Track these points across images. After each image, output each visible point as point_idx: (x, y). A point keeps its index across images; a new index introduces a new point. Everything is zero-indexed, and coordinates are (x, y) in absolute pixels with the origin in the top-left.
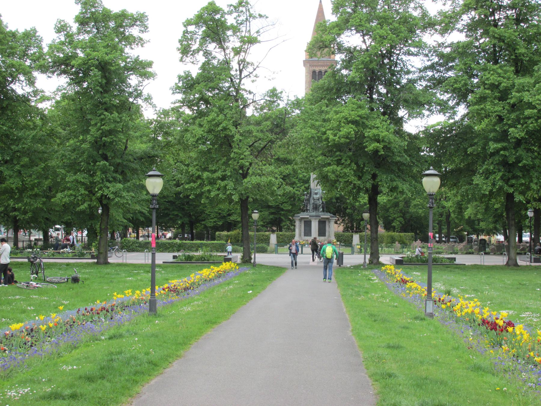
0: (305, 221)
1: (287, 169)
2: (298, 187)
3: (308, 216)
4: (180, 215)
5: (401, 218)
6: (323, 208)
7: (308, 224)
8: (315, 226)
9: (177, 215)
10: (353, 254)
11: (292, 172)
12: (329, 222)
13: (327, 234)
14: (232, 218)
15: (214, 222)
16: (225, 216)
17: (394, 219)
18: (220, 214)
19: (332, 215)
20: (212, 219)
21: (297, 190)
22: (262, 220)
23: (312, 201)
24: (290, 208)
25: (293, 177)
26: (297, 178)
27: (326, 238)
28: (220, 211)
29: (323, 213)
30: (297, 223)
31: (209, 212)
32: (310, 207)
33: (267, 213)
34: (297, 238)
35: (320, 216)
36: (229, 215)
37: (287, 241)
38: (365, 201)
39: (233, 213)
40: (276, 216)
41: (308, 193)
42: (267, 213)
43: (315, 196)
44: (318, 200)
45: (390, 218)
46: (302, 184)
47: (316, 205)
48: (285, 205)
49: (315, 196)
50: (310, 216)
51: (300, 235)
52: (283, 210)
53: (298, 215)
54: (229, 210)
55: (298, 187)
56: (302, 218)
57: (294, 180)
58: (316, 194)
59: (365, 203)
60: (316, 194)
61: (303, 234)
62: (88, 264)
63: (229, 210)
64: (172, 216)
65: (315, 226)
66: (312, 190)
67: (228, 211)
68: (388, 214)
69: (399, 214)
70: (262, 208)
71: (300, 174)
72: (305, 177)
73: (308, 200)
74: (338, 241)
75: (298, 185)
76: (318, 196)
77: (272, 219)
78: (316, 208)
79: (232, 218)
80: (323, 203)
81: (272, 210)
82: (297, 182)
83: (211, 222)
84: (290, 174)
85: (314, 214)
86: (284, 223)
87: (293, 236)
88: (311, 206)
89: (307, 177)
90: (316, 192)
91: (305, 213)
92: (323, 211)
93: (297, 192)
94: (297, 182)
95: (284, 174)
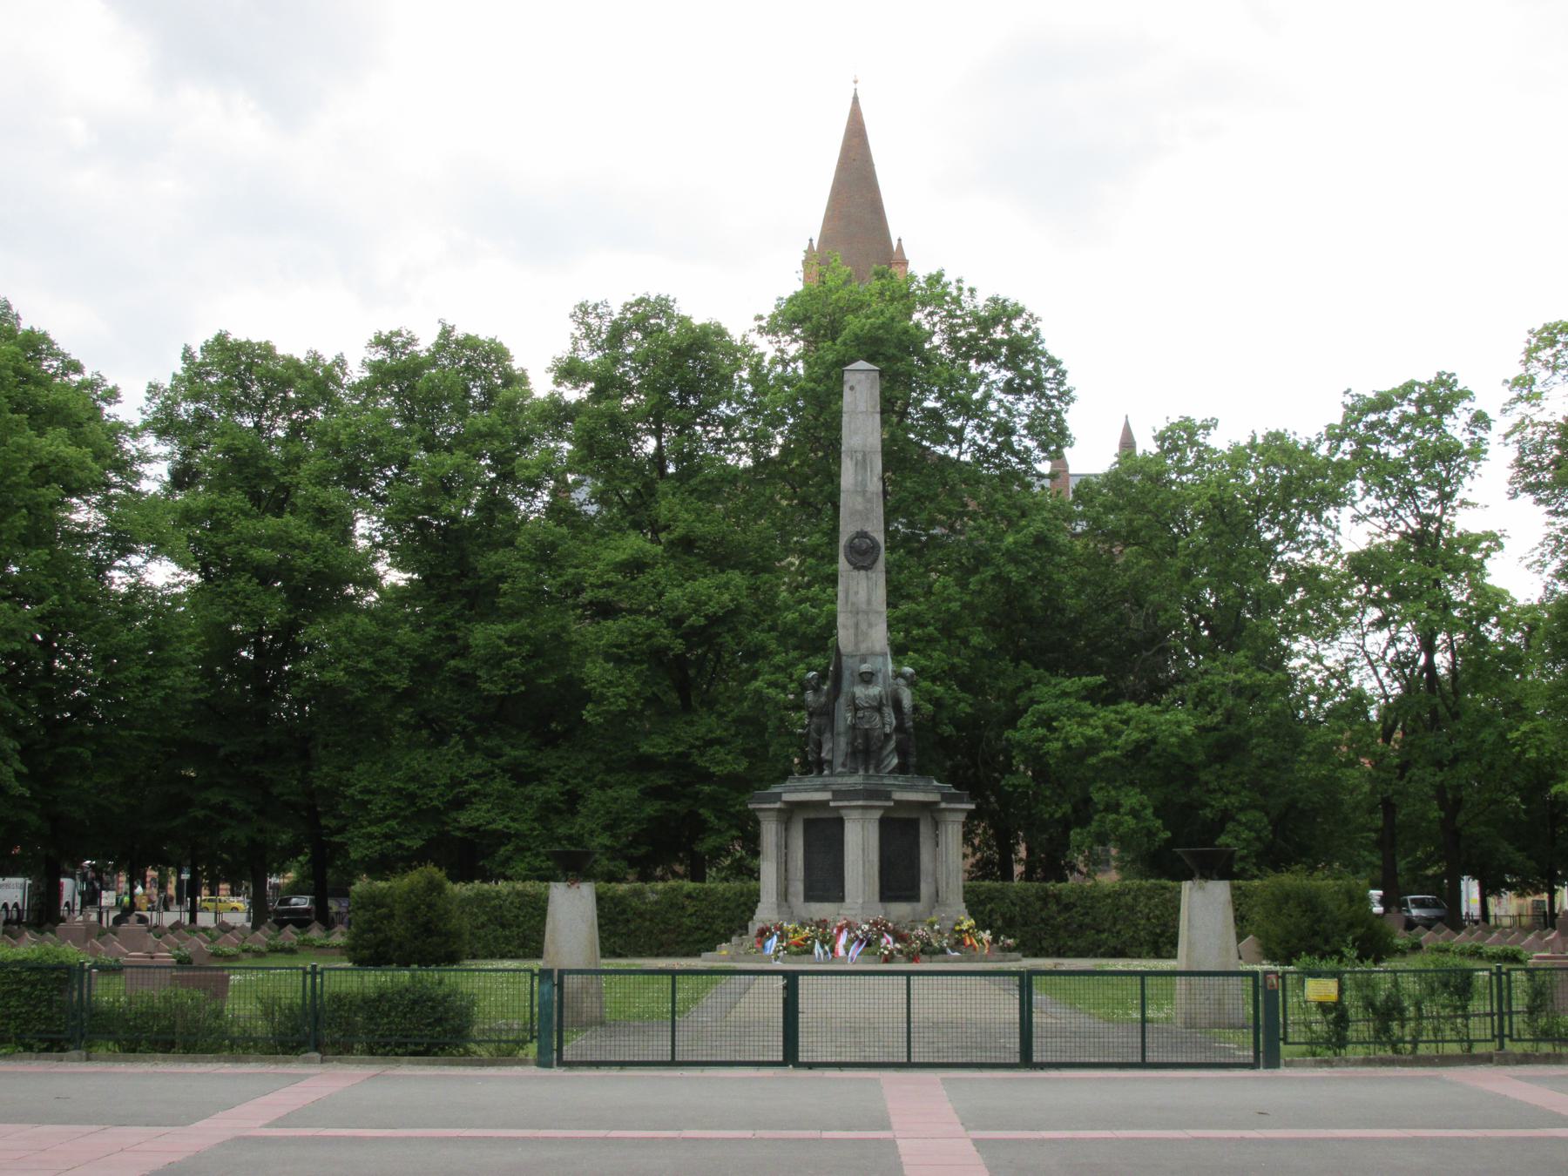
0: (809, 825)
1: (726, 586)
2: (778, 668)
3: (826, 796)
4: (237, 805)
5: (1258, 814)
6: (901, 751)
7: (824, 836)
8: (860, 844)
9: (224, 809)
10: (1273, 1061)
11: (749, 604)
12: (936, 825)
13: (925, 889)
14: (465, 818)
15: (387, 837)
16: (436, 808)
17: (1226, 816)
18: (412, 797)
19: (949, 788)
20: (380, 821)
21: (771, 684)
22: (606, 828)
23: (844, 717)
24: (741, 766)
25: (752, 626)
26: (772, 628)
27: (920, 907)
28: (413, 787)
29: (901, 780)
30: (770, 833)
31: (365, 791)
32: (836, 748)
33: (631, 793)
34: (766, 912)
35: (888, 796)
36: (459, 804)
37: (720, 926)
38: (1089, 732)
39: (475, 793)
40: (674, 806)
41: (823, 677)
42: (631, 793)
43: (860, 691)
44: (879, 709)
45: (1208, 813)
46: (794, 654)
47: (867, 734)
48: (720, 752)
49: (860, 691)
50: (837, 795)
51: (784, 895)
52: (707, 777)
53: (775, 789)
54: (455, 782)
55: (778, 668)
56: (795, 807)
57: (757, 636)
58: (867, 678)
59: (1090, 740)
60: (867, 678)
61: (798, 887)
62: (346, 969)
63: (455, 782)
64: (200, 814)
65: (860, 844)
66: (846, 662)
67: (450, 787)
68: (1195, 791)
69: (1246, 796)
70: (609, 770)
71: (788, 608)
72: (811, 621)
73: (826, 713)
74: (982, 925)
75: (778, 659)
76: (875, 690)
77: (651, 819)
78: (864, 752)
79: (465, 818)
80: (900, 728)
81: (658, 779)
82: (773, 646)
83: (370, 836)
84: (738, 610)
85: (856, 781)
86: (711, 842)
87: (750, 902)
88: (842, 742)
89: (822, 621)
90: (865, 667)
91: (812, 780)
92: (902, 769)
93: (772, 692)
94: (773, 646)
95: (711, 609)
